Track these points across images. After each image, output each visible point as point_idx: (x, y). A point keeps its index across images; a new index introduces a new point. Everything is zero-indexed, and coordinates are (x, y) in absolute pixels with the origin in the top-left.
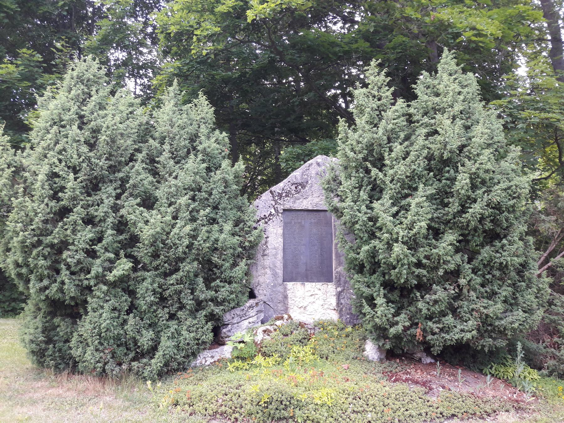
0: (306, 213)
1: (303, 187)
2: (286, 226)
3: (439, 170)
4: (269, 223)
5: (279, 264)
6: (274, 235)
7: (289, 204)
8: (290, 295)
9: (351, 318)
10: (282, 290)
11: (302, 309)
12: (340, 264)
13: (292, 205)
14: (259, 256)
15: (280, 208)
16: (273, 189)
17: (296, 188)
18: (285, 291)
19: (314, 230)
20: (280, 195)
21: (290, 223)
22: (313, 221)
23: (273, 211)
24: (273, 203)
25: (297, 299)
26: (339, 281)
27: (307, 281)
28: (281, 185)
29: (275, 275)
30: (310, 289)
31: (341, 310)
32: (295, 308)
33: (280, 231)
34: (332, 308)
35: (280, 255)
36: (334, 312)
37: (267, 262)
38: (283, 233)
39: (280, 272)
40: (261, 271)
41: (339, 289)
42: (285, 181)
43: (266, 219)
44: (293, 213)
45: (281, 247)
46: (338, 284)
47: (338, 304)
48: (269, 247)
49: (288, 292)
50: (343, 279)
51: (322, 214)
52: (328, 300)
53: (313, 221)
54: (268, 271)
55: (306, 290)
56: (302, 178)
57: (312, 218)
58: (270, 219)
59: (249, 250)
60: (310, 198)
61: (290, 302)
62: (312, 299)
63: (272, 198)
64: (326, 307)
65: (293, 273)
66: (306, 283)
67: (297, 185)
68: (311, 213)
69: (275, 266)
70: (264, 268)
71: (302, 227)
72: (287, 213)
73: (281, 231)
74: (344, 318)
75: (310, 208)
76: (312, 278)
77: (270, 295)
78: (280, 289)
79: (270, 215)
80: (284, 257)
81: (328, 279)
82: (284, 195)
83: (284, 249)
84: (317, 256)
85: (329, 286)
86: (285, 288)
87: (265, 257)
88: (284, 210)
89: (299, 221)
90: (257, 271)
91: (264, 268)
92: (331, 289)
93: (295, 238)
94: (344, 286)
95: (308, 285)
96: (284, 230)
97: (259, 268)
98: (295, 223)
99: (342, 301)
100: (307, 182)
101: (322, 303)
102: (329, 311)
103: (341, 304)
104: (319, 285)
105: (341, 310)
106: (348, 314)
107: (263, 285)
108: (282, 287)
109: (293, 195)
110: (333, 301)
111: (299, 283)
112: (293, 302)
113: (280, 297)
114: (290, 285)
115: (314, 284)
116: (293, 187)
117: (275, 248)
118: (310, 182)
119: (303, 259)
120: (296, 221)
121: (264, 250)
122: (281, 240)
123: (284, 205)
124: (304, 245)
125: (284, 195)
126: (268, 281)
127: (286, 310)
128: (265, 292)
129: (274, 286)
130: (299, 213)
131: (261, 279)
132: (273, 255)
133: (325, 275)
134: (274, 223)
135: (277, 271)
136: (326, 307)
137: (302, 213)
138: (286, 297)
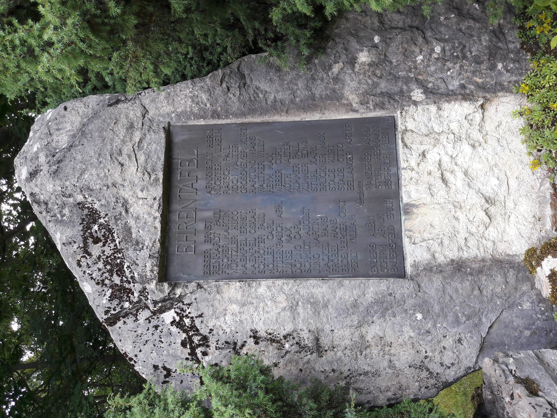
0: (176, 206)
1: (92, 216)
2: (218, 270)
3: (390, 75)
4: (204, 331)
5: (346, 290)
6: (249, 310)
7: (143, 263)
8: (452, 254)
9: (504, 59)
10: (437, 281)
11: (492, 210)
12: (335, 98)
13: (145, 253)
14: (321, 365)
15: (156, 291)
16: (101, 316)
17: (96, 241)
18: (439, 269)
19: (232, 178)
20: (120, 293)
21: (207, 255)
22: (201, 184)
23: (169, 316)
24: (144, 315)
25: (462, 227)
26: (390, 96)
27: (397, 195)
28: (87, 288)
29: (384, 307)
30: (423, 188)
31: (482, 87)
32: (492, 233)
33: (233, 290)
34: (478, 116)
35: (317, 288)
36: (491, 109)
37: (340, 334)
38: (240, 279)
39: (374, 288)
40: (375, 358)
41: (418, 94)
42: (77, 273)
43: (195, 341)
44: (174, 249)
45: (288, 285)
46: (401, 98)
47: (467, 97)
48: (289, 328)
49: (441, 259)
50: (383, 86)
51: (179, 155)
52: (454, 126)
53: (201, 184)
54: (372, 332)
55: (427, 198)
56: (70, 223)
57: (194, 188)
58: (193, 327)
59: (64, 405)
60: (126, 194)
61: (473, 251)
62: (457, 181)
63: (130, 320)
64: (476, 135)
65: (372, 242)
66: (405, 199)
67: (88, 238)
68: (176, 192)
69: (355, 305)
70: (362, 346)
71: (220, 216)
72: (174, 269)
73: (236, 285)
74: (506, 77)
75: (158, 191)
76: (387, 183)
77: (457, 322)
78: (432, 287)
79: (179, 324)
80: (322, 275)
81: (388, 128)
82: (117, 280)
83: (294, 276)
84: (312, 168)
85: (410, 125)
86: (431, 269)
87: (325, 341)
88: (164, 275)
89: (201, 226)
90: (376, 374)
91: (362, 346)
92: (417, 120)
93: (259, 240)
94: (407, 80)
95: (410, 192)
96: (230, 278)
97: (363, 365)
98: (208, 240)
99: (454, 84)
100: (81, 205)
101: (467, 148)
102: (489, 126)
103: (463, 87)
104: (407, 159)
105: (482, 87)
106: (493, 67)
107: (425, 348)
108: (424, 282)
109: (117, 250)
110: (457, 111)
111: (407, 224)
112: (472, 242)
113: (462, 286)
114: (414, 254)
115: (405, 175)
116: (95, 250)
117: (293, 308)
118: (80, 198)
119: (323, 212)
120: (201, 238)
121: (301, 347)
122: (263, 287)
123: (144, 280)
124: (278, 209)
125: (117, 280)
126: (408, 332)
127: (501, 264)
128: (449, 342)
129: (424, 307)
130: (174, 229)
131: (404, 357)
132: (317, 313)
133: (375, 143)
134: (208, 312)
135: (370, 297)
136: (476, 135)
137: (175, 217)
138: (459, 267)
